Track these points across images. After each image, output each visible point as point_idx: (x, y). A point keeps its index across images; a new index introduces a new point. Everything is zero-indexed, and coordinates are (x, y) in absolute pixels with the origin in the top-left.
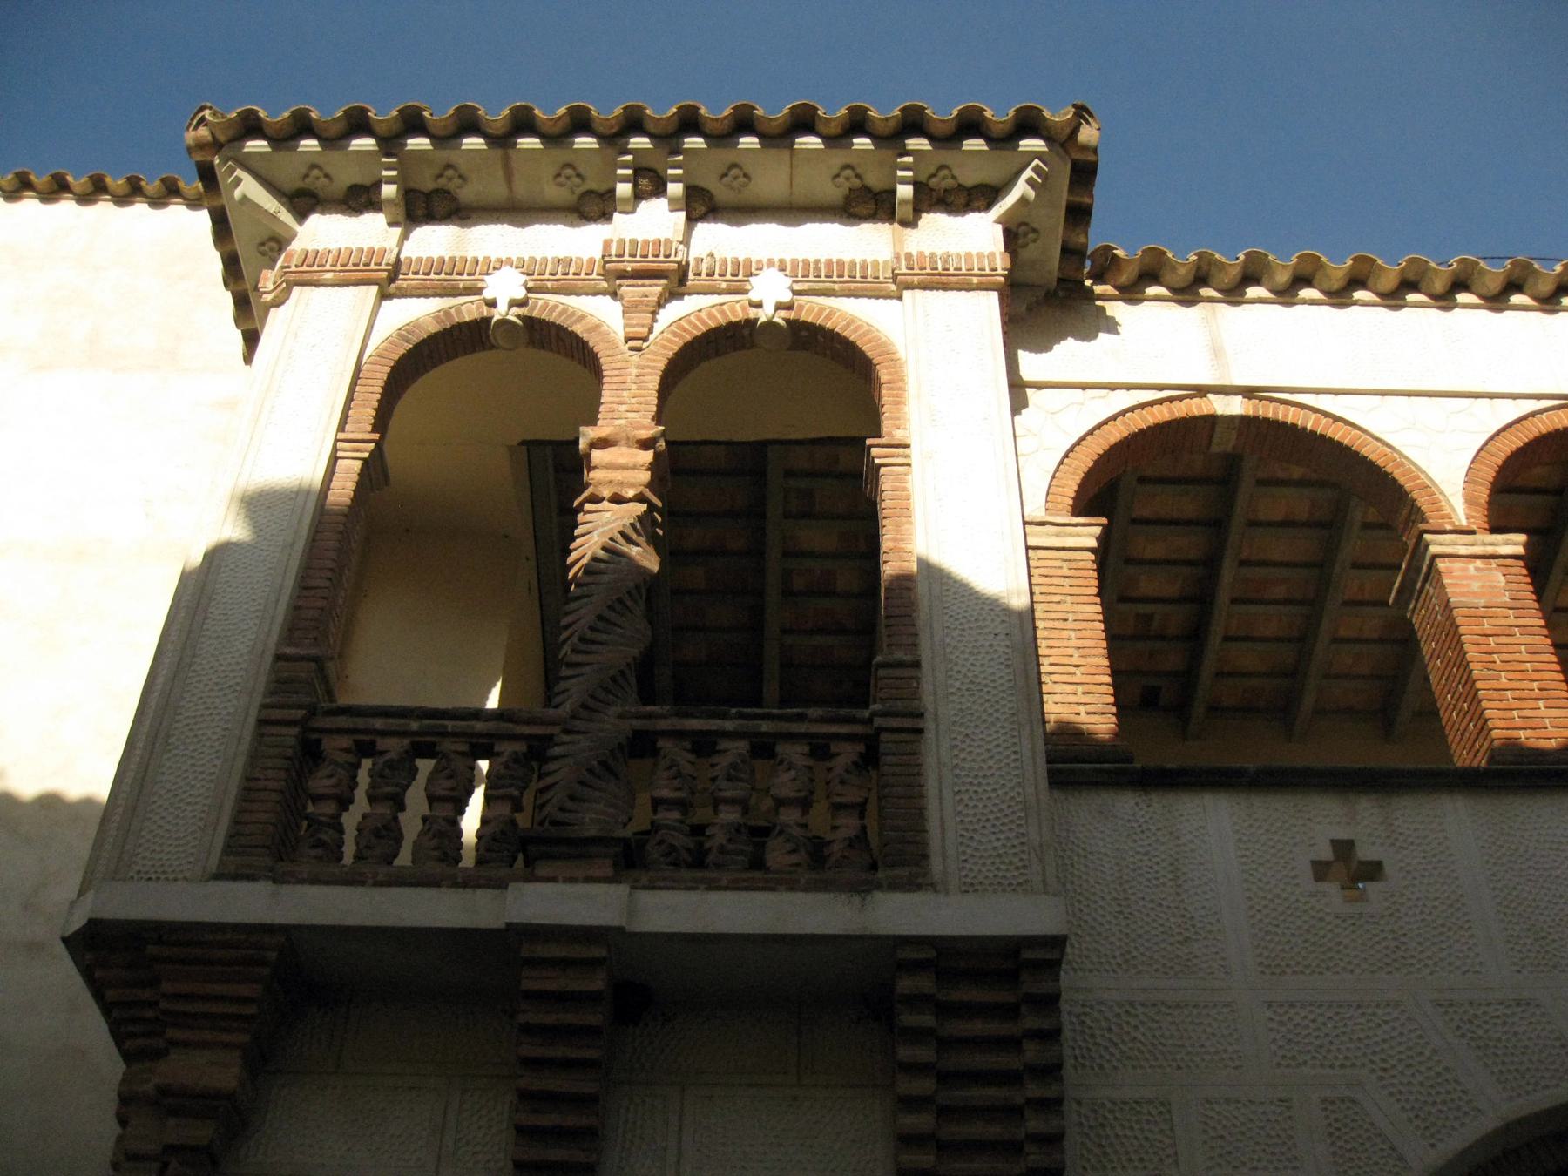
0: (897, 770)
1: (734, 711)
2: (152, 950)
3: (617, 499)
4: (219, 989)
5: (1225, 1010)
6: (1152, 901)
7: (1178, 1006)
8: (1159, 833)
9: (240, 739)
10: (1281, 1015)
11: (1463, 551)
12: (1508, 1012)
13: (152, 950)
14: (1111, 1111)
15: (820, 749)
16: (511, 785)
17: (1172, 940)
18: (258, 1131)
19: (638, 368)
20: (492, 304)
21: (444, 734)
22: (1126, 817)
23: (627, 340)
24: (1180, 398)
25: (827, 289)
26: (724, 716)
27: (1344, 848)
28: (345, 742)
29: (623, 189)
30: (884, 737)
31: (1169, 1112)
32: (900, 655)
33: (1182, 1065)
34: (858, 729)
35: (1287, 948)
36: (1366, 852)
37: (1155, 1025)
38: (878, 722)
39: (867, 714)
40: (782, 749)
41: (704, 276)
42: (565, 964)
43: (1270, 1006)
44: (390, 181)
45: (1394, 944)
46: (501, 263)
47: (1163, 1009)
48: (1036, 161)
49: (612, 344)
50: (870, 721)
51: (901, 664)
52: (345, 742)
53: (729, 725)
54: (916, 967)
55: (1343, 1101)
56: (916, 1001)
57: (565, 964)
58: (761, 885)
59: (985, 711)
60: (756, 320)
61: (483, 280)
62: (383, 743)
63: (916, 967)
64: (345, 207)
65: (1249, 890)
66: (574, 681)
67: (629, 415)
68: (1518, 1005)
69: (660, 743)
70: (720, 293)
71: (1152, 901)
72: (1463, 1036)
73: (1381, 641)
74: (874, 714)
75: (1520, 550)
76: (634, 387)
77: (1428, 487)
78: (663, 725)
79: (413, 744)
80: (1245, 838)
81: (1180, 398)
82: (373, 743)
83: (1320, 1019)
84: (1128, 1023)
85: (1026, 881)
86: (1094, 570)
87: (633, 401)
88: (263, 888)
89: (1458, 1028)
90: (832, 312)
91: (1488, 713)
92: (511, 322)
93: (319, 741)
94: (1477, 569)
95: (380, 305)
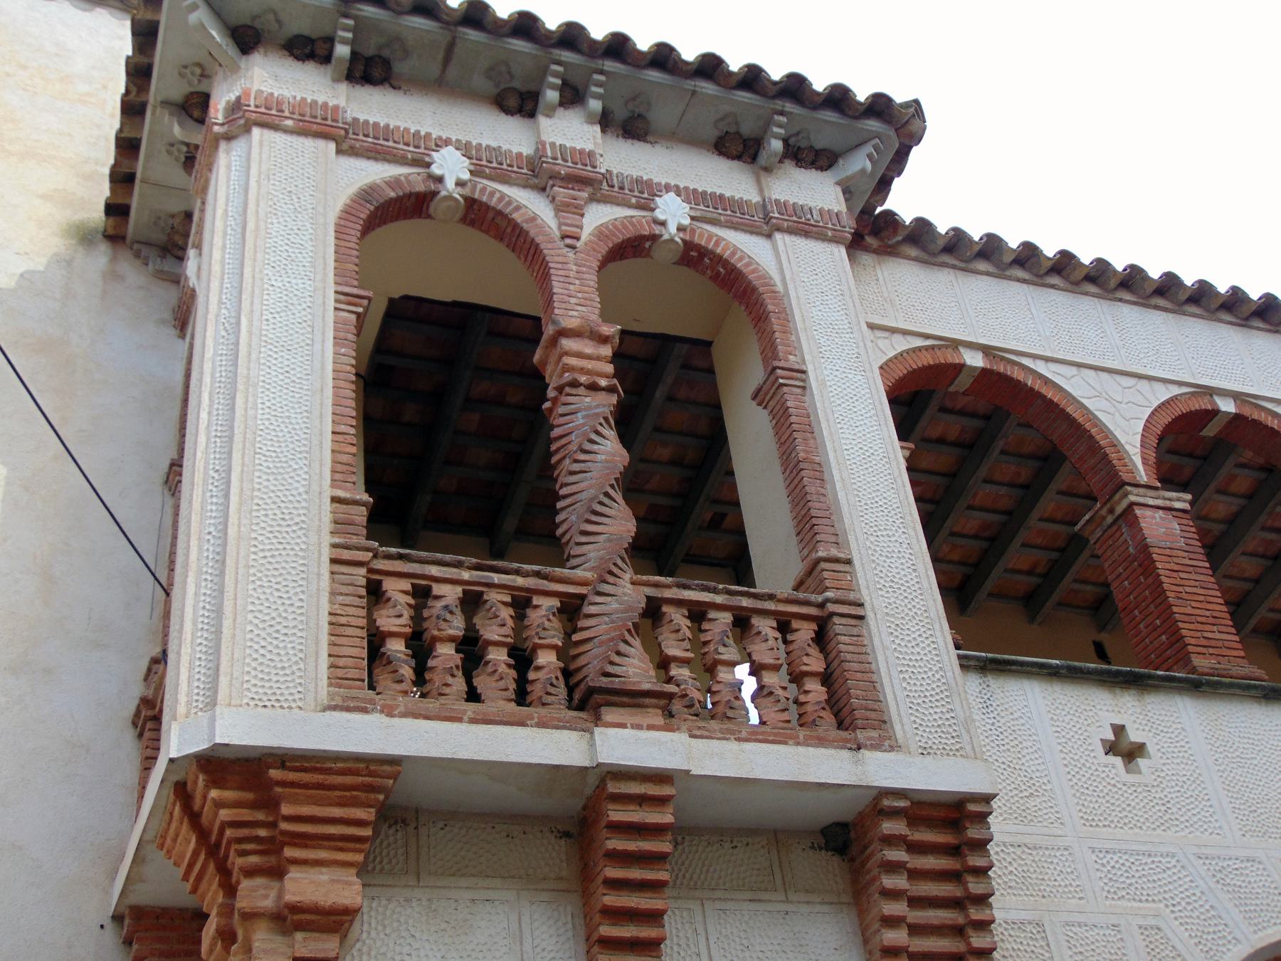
0: (851, 648)
1: (721, 586)
2: (274, 773)
3: (593, 387)
4: (337, 812)
5: (1066, 853)
6: (1003, 763)
7: (1035, 848)
8: (999, 709)
9: (319, 575)
10: (1101, 859)
11: (1151, 502)
12: (1243, 866)
13: (274, 773)
14: (1006, 929)
15: (698, 614)
16: (553, 637)
17: (1021, 795)
18: (358, 940)
19: (576, 265)
20: (440, 179)
21: (490, 585)
22: (975, 694)
23: (563, 237)
24: (947, 347)
25: (586, 178)
26: (715, 591)
27: (1119, 730)
28: (406, 585)
29: (552, 96)
30: (836, 620)
31: (1044, 931)
32: (834, 552)
33: (1046, 894)
34: (813, 611)
35: (1096, 806)
36: (1134, 736)
37: (1022, 862)
38: (831, 607)
39: (820, 599)
40: (756, 621)
41: (616, 189)
42: (642, 800)
43: (1093, 852)
44: (344, 41)
45: (1163, 808)
46: (447, 142)
47: (1027, 850)
48: (877, 141)
49: (551, 241)
50: (821, 606)
51: (837, 560)
52: (406, 585)
53: (719, 599)
54: (894, 813)
55: (1152, 928)
56: (890, 841)
57: (642, 800)
58: (771, 738)
59: (906, 606)
60: (661, 236)
61: (428, 155)
62: (437, 589)
63: (894, 813)
64: (287, 53)
65: (1064, 758)
66: (590, 547)
67: (579, 308)
68: (1248, 861)
69: (665, 609)
70: (630, 206)
71: (1003, 763)
72: (1218, 882)
73: (975, 537)
74: (827, 600)
75: (1186, 506)
76: (577, 282)
77: (1115, 444)
78: (668, 594)
79: (464, 592)
80: (1055, 718)
81: (940, 347)
82: (429, 588)
83: (1128, 864)
84: (1004, 859)
85: (961, 748)
86: (353, 366)
87: (580, 295)
88: (376, 719)
89: (1214, 875)
90: (719, 240)
91: (1184, 632)
92: (456, 200)
93: (380, 582)
94: (1161, 518)
95: (978, 349)
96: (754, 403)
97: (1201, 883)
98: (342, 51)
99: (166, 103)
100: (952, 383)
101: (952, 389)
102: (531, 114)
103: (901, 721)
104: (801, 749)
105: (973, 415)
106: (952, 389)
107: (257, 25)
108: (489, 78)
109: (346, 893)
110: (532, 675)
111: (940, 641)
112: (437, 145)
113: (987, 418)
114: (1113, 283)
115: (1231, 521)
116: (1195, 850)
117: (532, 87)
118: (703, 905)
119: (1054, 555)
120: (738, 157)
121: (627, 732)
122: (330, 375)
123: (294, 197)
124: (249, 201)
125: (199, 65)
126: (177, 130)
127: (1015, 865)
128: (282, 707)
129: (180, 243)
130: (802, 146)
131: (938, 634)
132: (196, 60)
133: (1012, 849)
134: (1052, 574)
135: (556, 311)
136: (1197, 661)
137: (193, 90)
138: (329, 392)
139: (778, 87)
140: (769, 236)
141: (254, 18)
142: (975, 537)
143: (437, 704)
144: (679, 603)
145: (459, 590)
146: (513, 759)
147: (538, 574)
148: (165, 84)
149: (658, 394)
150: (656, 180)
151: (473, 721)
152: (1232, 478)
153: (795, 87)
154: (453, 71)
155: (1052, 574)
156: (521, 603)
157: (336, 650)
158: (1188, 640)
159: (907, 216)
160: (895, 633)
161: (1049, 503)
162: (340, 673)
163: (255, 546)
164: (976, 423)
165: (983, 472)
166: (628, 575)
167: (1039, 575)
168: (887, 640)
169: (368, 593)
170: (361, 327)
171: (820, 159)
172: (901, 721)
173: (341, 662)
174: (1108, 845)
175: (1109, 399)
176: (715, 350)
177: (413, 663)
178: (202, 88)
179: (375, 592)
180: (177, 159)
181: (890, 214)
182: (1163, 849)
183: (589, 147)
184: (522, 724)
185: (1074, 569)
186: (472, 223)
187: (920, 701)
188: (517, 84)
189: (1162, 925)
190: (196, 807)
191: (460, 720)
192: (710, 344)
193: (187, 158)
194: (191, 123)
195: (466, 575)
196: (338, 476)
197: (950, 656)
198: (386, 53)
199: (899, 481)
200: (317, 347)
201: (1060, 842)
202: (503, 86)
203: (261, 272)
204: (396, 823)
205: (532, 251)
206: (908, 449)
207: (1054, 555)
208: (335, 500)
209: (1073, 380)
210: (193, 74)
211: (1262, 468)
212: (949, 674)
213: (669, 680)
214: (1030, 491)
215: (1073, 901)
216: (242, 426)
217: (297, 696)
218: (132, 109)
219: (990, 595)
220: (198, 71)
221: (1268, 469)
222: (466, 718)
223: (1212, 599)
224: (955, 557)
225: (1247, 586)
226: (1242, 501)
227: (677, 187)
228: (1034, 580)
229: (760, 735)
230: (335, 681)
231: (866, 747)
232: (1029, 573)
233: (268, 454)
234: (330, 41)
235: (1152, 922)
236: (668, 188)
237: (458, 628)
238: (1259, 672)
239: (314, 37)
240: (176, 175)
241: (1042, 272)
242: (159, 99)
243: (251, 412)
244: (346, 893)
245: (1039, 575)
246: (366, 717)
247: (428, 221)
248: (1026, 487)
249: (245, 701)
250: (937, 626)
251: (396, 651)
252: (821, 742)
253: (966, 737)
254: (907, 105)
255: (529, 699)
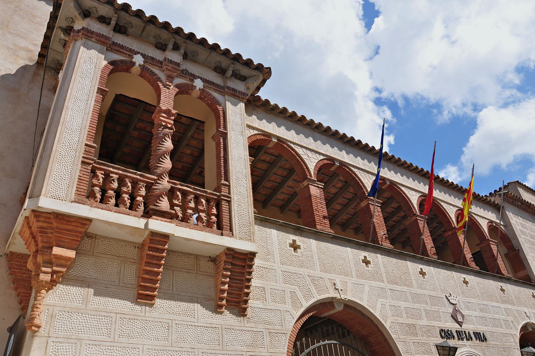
5: (274, 271)
9: (77, 164)
15: (185, 194)
46: (139, 53)
73: (270, 188)
88: (87, 207)
96: (212, 139)
97: (307, 282)
98: (113, 23)
99: (60, 27)
100: (268, 145)
101: (268, 146)
102: (164, 51)
103: (235, 230)
104: (207, 233)
105: (274, 155)
106: (268, 146)
107: (91, 11)
108: (154, 38)
109: (70, 254)
110: (134, 202)
111: (250, 210)
112: (136, 53)
113: (277, 157)
114: (314, 126)
115: (335, 194)
116: (308, 274)
117: (166, 43)
118: (173, 272)
119: (290, 196)
120: (220, 73)
121: (159, 221)
122: (92, 110)
123: (91, 59)
124: (78, 58)
125: (72, 18)
126: (62, 35)
127: (260, 272)
128: (60, 199)
129: (59, 68)
130: (238, 73)
131: (250, 209)
132: (71, 17)
133: (260, 268)
134: (288, 201)
135: (160, 104)
136: (317, 226)
137: (69, 25)
138: (90, 114)
139: (234, 56)
140: (224, 96)
141: (90, 8)
142: (270, 188)
143: (105, 206)
144: (180, 190)
145: (118, 176)
146: (125, 224)
147: (141, 175)
148: (61, 22)
149: (189, 135)
150: (196, 74)
151: (115, 212)
152: (337, 183)
153: (238, 57)
154: (144, 34)
155: (288, 201)
156: (135, 183)
157: (79, 186)
158: (316, 221)
159: (263, 98)
160: (238, 207)
161: (290, 183)
162: (79, 193)
163: (60, 153)
164: (274, 158)
165: (274, 171)
166: (167, 179)
167: (285, 201)
168: (236, 208)
169: (91, 172)
170: (104, 99)
171: (243, 79)
172: (235, 230)
173: (79, 190)
174: (286, 270)
175: (308, 156)
176: (205, 124)
177: (101, 193)
178: (72, 25)
179: (93, 171)
180: (61, 44)
181: (259, 97)
182: (300, 273)
183: (178, 62)
184: (129, 215)
185: (294, 201)
186: (142, 77)
187: (241, 225)
188: (161, 41)
189: (295, 291)
190: (31, 224)
191: (111, 211)
192: (204, 123)
193: (64, 44)
194: (66, 34)
195: (120, 172)
196: (88, 138)
197: (252, 215)
198: (126, 26)
199: (247, 167)
200: (89, 102)
201: (274, 268)
202: (158, 41)
203: (77, 78)
204: (89, 237)
205: (157, 87)
206: (252, 159)
207: (290, 196)
208: (86, 145)
209: (299, 150)
210: (69, 20)
211: (344, 182)
212: (251, 220)
213: (174, 210)
214: (285, 179)
215: (274, 283)
216: (63, 120)
217: (65, 197)
218: (50, 27)
219: (271, 205)
220: (71, 20)
221: (346, 182)
222: (113, 211)
223: (324, 211)
224: (264, 193)
225: (337, 212)
226: (338, 190)
227: (201, 77)
228: (284, 202)
229: (195, 227)
230: (78, 194)
231: (224, 235)
232: (283, 200)
233: (69, 128)
234: (111, 19)
235: (293, 290)
236: (199, 77)
237: (115, 186)
238: (333, 232)
239: (106, 17)
240: (60, 49)
241: (296, 120)
242: (59, 26)
243: (66, 116)
244: (70, 254)
245: (285, 201)
246: (84, 206)
247: (129, 74)
248: (285, 177)
249: (49, 196)
250: (250, 207)
251: (96, 189)
252: (212, 232)
253: (252, 237)
254: (267, 68)
255: (133, 209)
